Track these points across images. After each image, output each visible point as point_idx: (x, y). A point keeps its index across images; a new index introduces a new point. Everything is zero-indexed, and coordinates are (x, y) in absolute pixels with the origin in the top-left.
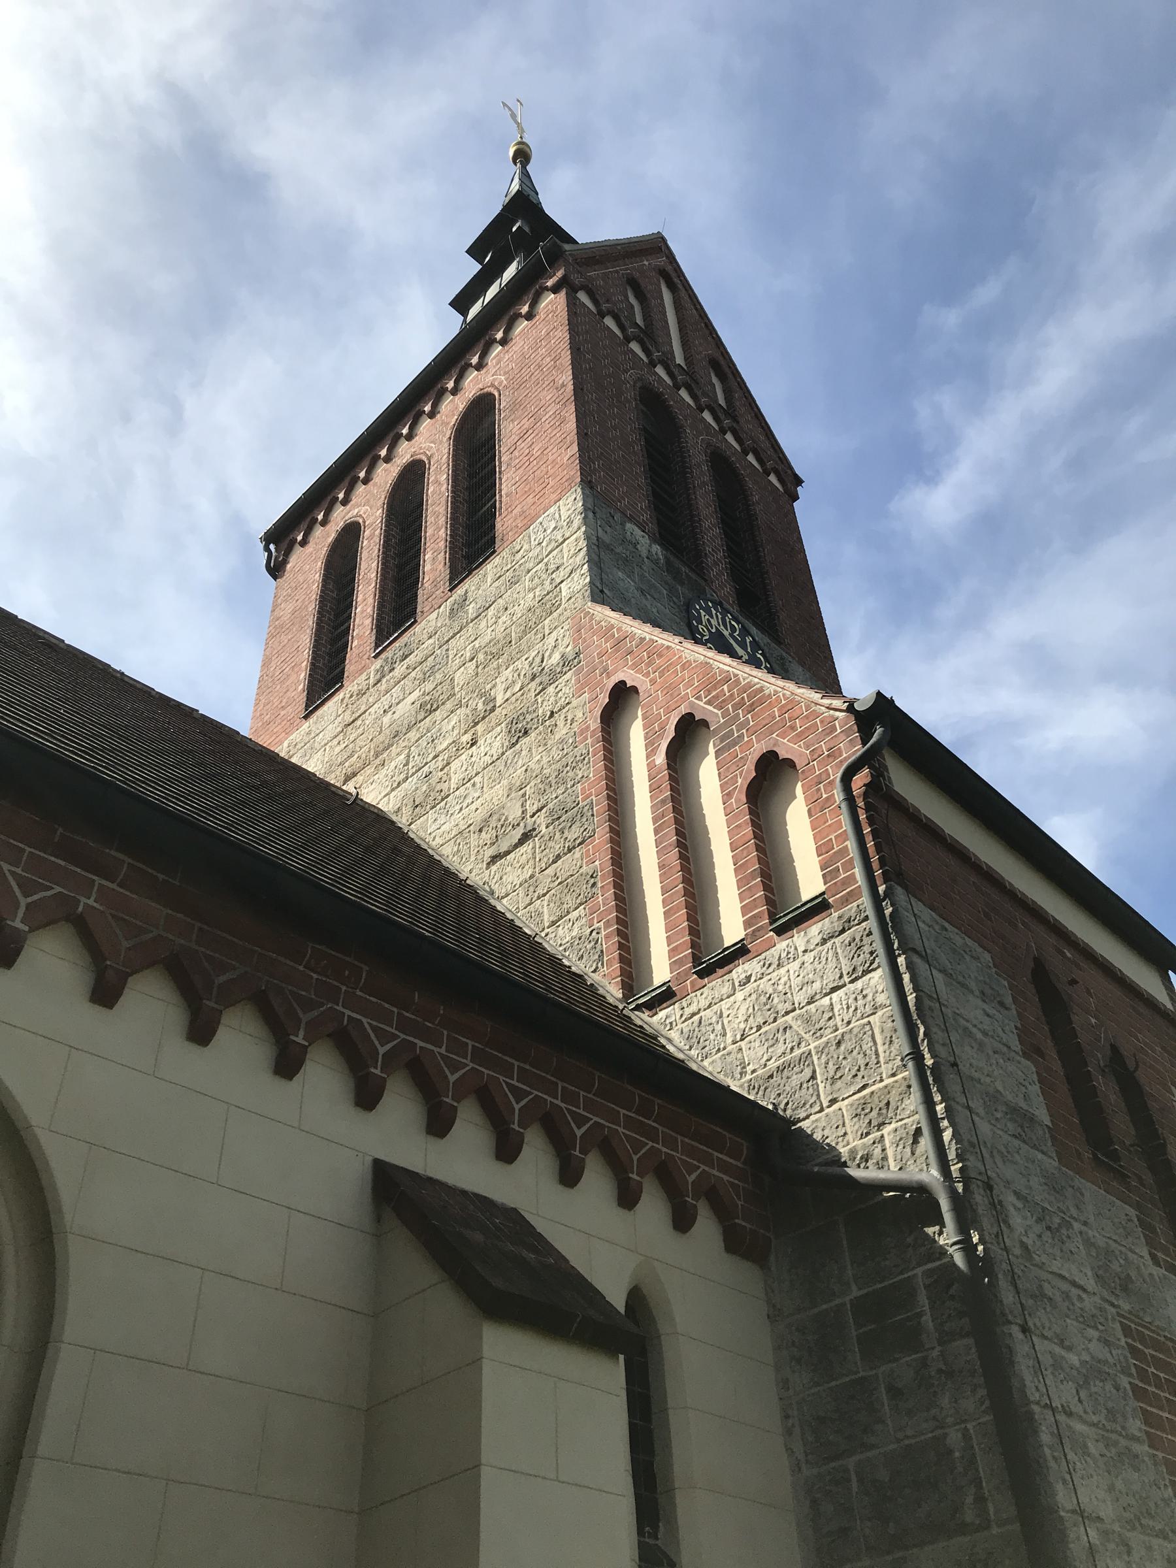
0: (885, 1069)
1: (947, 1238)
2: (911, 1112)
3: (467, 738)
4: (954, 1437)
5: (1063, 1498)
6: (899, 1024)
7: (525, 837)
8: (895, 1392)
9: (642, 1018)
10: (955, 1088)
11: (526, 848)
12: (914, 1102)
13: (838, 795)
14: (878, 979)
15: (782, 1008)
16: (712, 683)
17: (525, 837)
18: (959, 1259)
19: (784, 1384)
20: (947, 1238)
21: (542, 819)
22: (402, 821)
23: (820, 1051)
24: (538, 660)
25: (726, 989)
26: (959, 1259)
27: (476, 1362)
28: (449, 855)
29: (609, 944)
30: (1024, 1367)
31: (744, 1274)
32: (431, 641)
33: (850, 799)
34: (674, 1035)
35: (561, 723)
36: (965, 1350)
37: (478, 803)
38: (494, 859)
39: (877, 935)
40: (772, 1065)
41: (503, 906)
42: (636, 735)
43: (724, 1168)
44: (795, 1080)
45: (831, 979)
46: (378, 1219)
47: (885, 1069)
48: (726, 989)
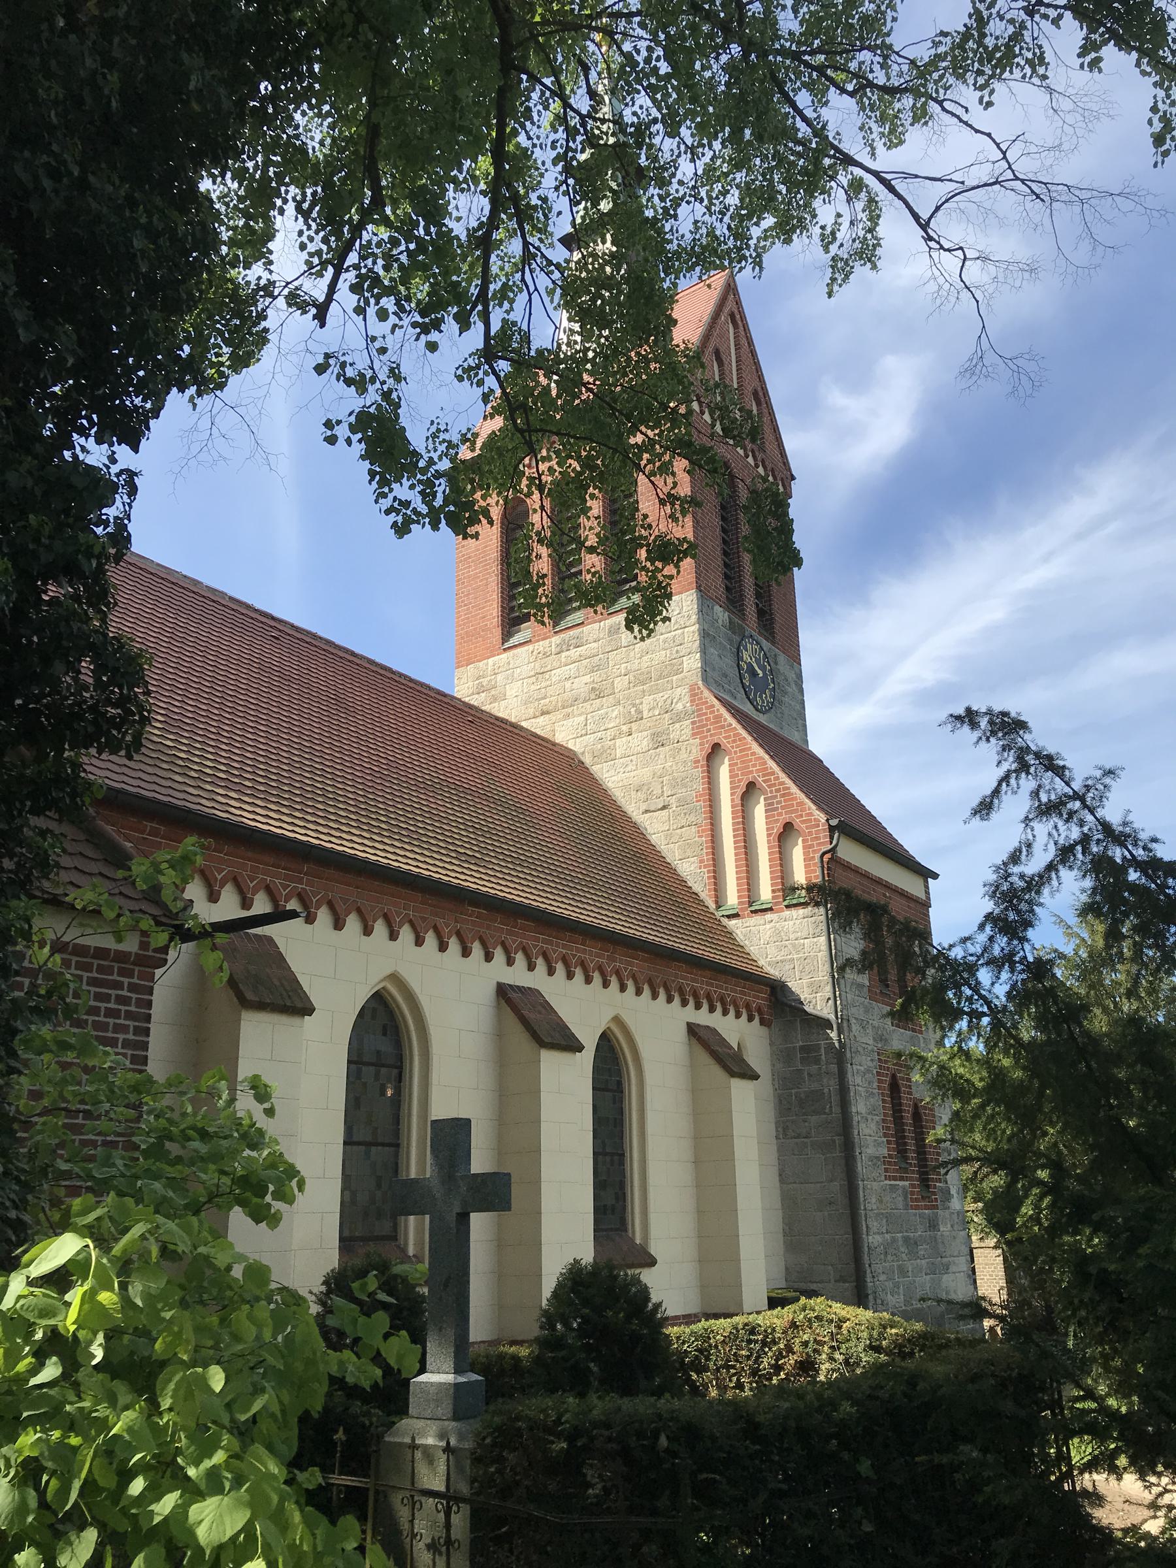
0: (821, 974)
1: (833, 1035)
2: (827, 991)
3: (625, 728)
4: (826, 1090)
5: (854, 1110)
6: (828, 959)
7: (664, 808)
8: (810, 1075)
9: (725, 921)
10: (842, 986)
11: (664, 812)
12: (829, 988)
13: (817, 860)
14: (823, 940)
15: (785, 938)
16: (768, 773)
17: (664, 808)
18: (837, 1045)
19: (773, 1065)
20: (833, 1035)
21: (673, 800)
22: (587, 760)
23: (798, 959)
24: (669, 701)
25: (762, 922)
26: (837, 1045)
27: (730, 1088)
28: (618, 795)
29: (706, 874)
30: (849, 1075)
31: (764, 1031)
32: (595, 645)
33: (822, 861)
34: (738, 932)
35: (683, 749)
36: (834, 1068)
37: (632, 774)
38: (647, 811)
39: (825, 923)
40: (779, 958)
41: (654, 839)
42: (724, 772)
43: (762, 999)
44: (787, 967)
45: (805, 934)
46: (690, 1045)
47: (821, 974)
48: (762, 922)
